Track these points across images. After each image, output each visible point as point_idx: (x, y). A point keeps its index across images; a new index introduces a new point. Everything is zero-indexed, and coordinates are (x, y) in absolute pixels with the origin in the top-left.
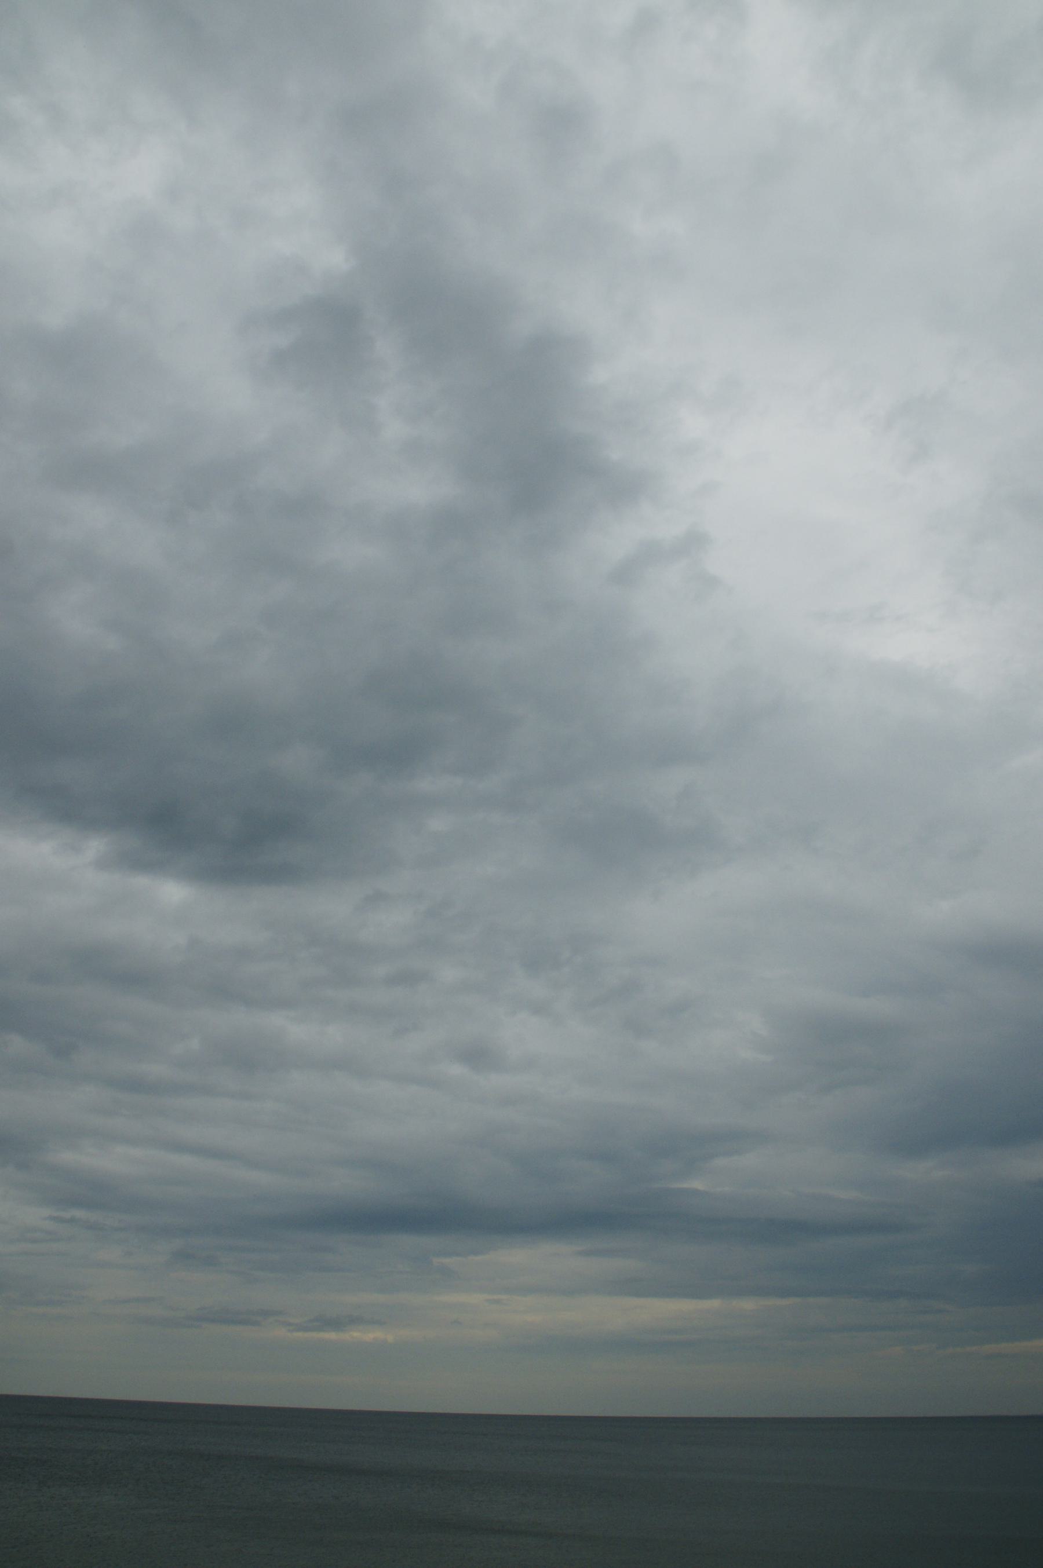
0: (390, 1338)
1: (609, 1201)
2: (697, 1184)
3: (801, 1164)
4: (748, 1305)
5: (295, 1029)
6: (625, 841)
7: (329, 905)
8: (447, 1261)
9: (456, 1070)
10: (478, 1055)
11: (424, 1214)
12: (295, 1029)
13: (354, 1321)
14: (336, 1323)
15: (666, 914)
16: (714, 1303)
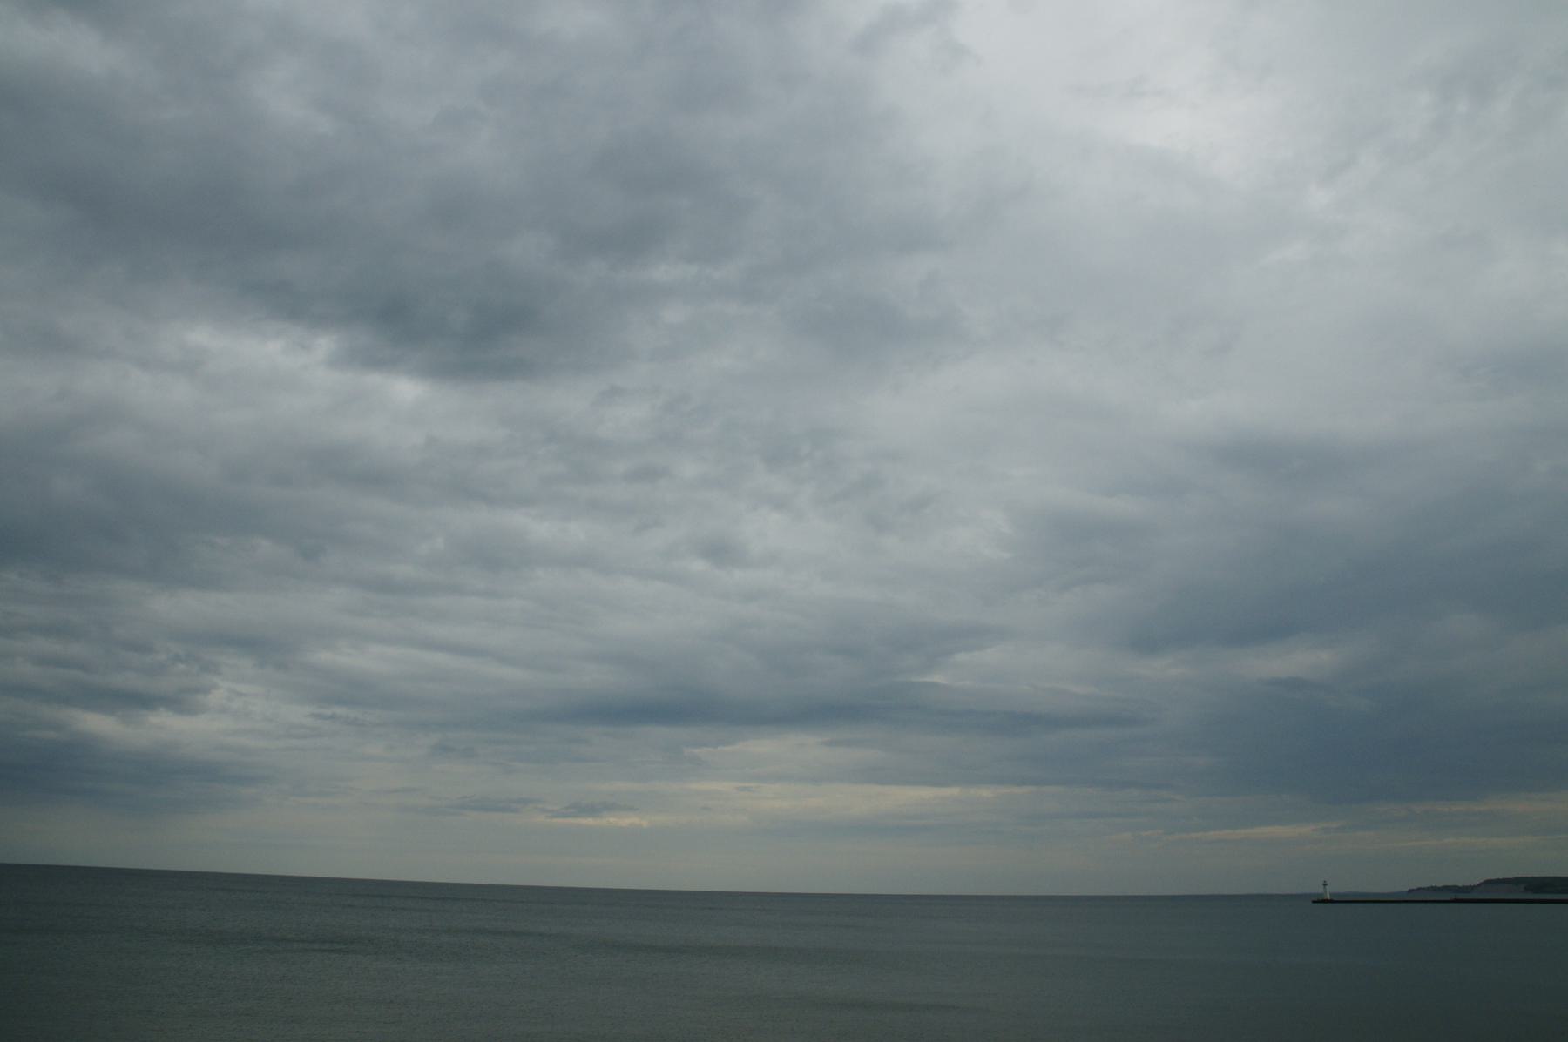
0: (645, 823)
1: (851, 693)
2: (938, 678)
3: (1039, 657)
4: (985, 792)
5: (539, 528)
6: (863, 332)
7: (567, 400)
8: (696, 751)
9: (699, 566)
10: (721, 552)
11: (674, 706)
12: (539, 528)
13: (610, 807)
14: (592, 810)
15: (903, 409)
16: (954, 791)
